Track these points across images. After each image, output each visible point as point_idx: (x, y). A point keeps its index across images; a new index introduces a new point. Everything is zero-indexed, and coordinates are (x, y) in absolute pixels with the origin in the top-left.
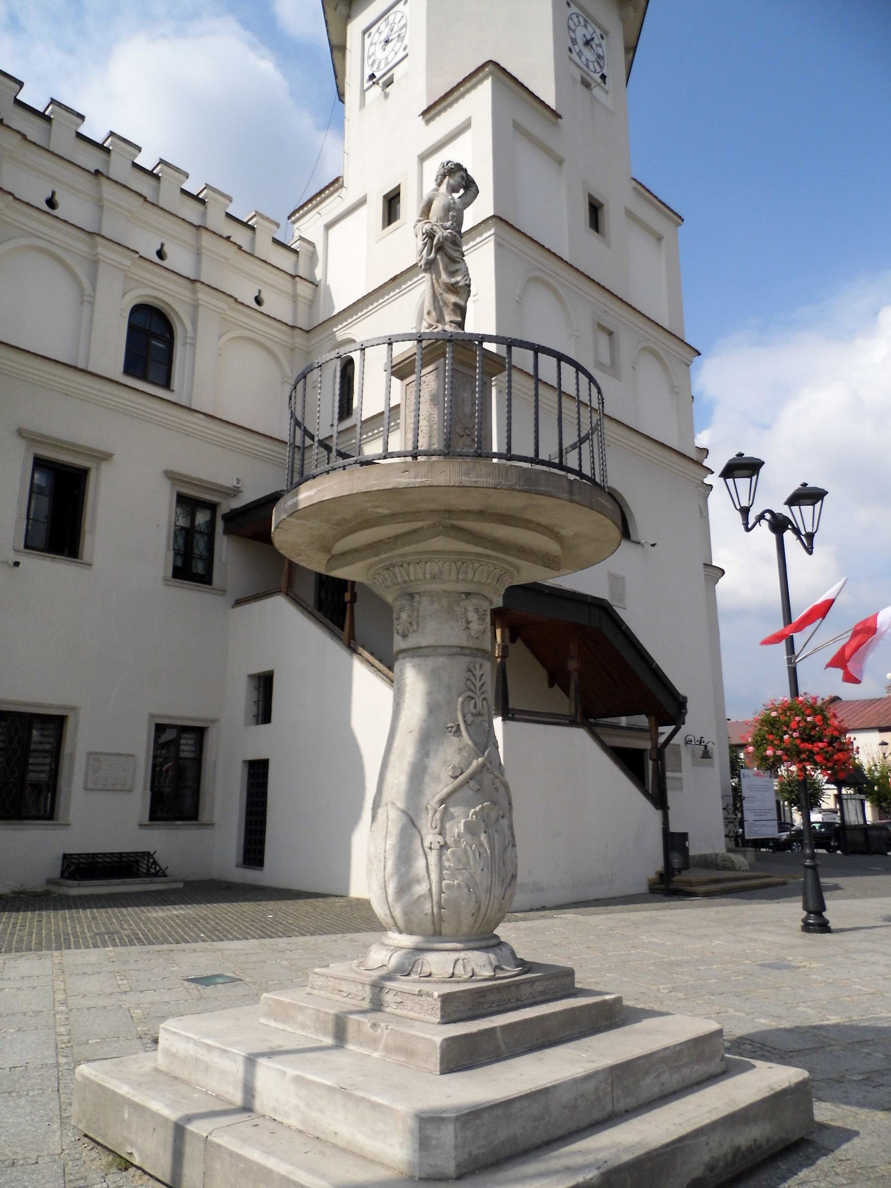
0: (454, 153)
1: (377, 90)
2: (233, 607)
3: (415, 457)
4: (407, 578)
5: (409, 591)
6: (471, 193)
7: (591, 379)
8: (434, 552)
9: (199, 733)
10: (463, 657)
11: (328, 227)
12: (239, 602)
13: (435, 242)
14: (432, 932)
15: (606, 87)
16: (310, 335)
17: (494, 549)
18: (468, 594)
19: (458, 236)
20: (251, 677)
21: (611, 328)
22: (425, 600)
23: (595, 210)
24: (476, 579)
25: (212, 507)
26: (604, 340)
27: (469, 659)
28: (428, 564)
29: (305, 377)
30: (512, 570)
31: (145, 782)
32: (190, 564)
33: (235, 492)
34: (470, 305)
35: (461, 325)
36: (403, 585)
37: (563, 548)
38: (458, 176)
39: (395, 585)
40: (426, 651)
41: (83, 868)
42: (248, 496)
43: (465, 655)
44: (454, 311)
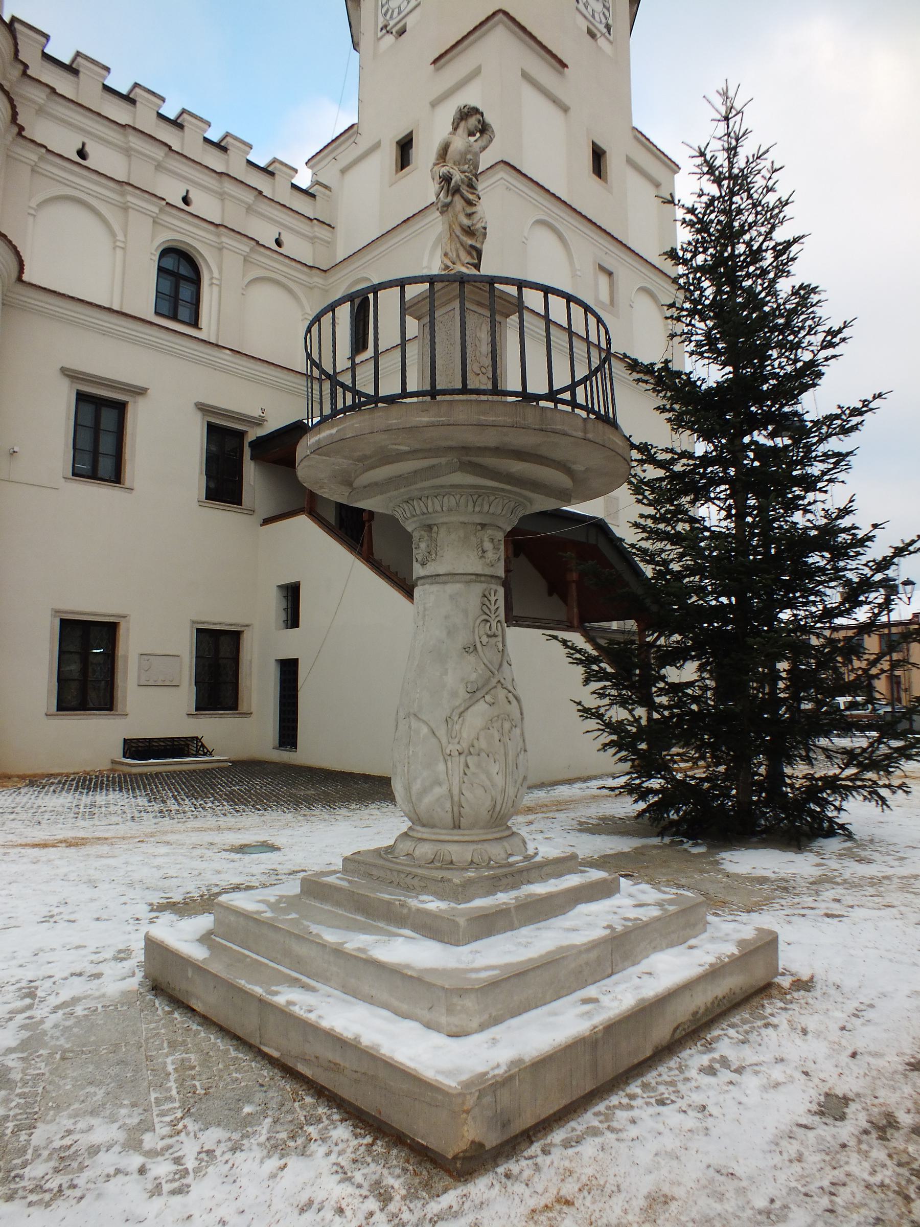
0: (470, 97)
1: (390, 39)
2: (261, 525)
3: (433, 398)
4: (425, 511)
5: (430, 522)
6: (486, 137)
7: (599, 320)
8: (452, 486)
9: (235, 637)
10: (479, 584)
11: (343, 171)
12: (266, 522)
13: (452, 185)
14: (452, 826)
15: (611, 38)
16: (327, 274)
17: (509, 483)
18: (483, 526)
19: (474, 179)
20: (280, 587)
21: (611, 269)
22: (443, 530)
23: (598, 155)
24: (491, 511)
25: (241, 435)
26: (603, 280)
27: (484, 586)
28: (446, 498)
29: (319, 321)
30: (525, 501)
31: (190, 679)
32: (223, 486)
33: (258, 422)
34: (486, 249)
35: (477, 267)
36: (421, 517)
37: (573, 481)
38: (473, 121)
39: (414, 516)
40: (445, 578)
41: (137, 749)
42: (274, 424)
43: (481, 582)
44: (469, 254)
